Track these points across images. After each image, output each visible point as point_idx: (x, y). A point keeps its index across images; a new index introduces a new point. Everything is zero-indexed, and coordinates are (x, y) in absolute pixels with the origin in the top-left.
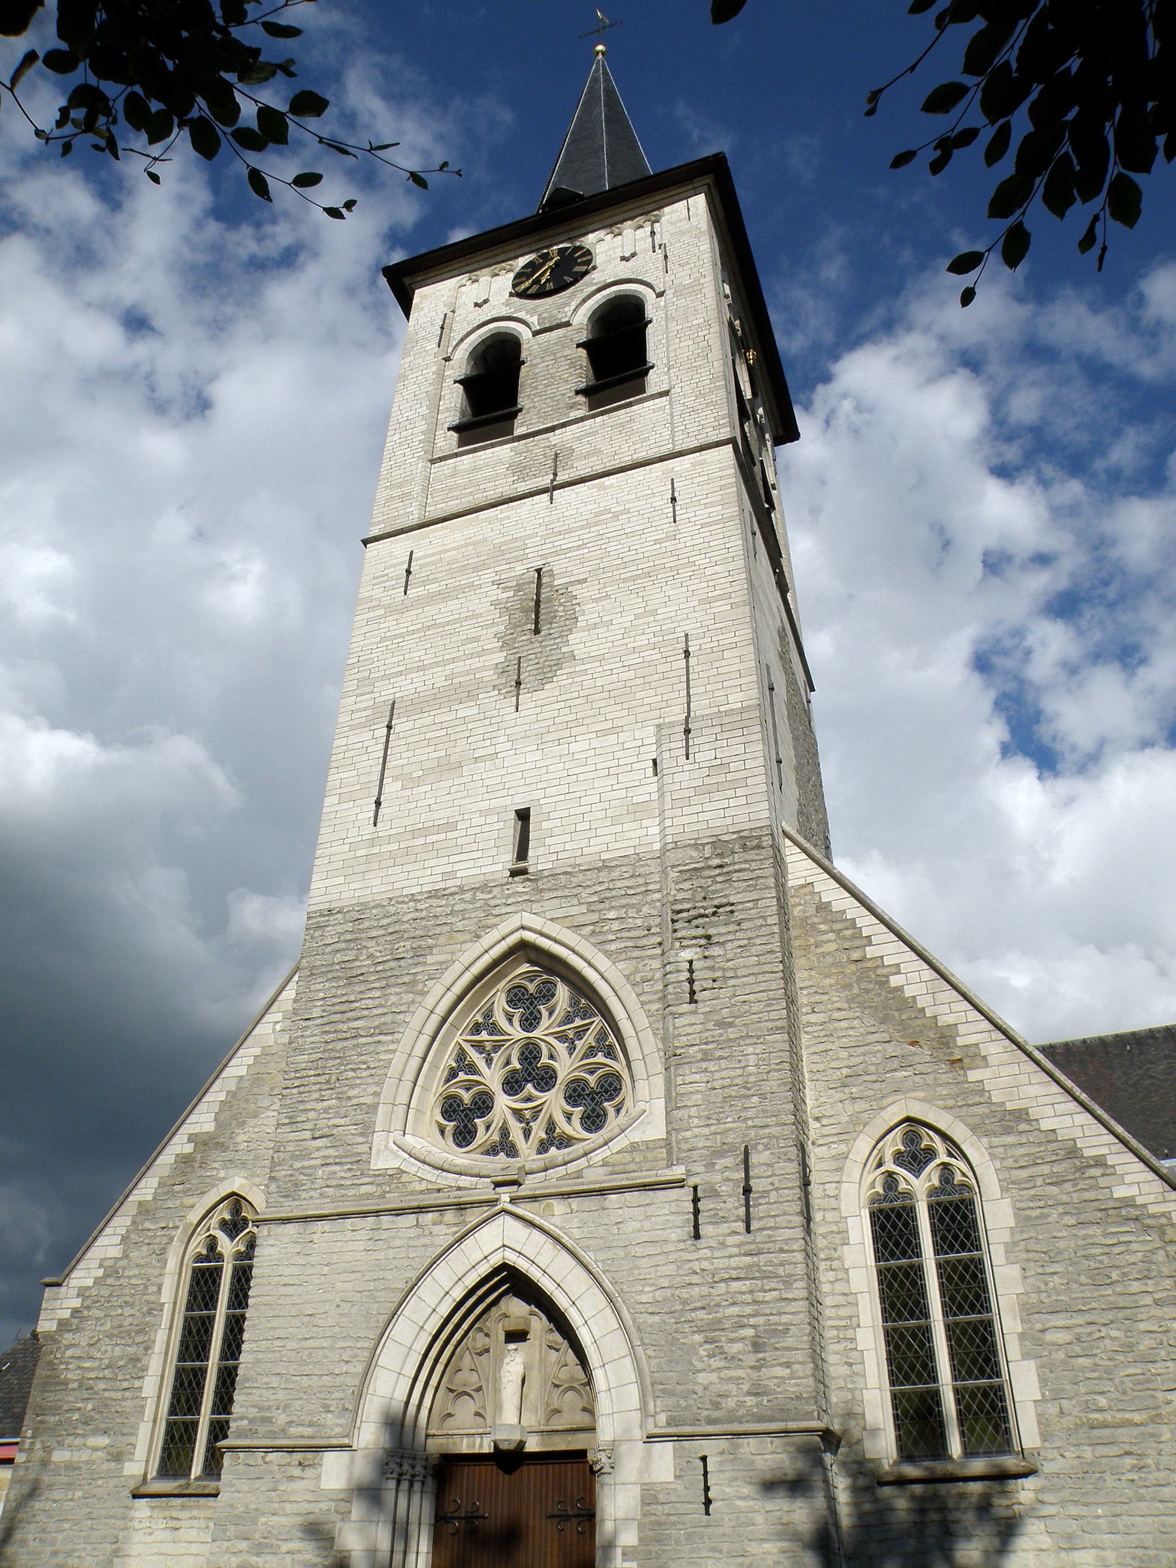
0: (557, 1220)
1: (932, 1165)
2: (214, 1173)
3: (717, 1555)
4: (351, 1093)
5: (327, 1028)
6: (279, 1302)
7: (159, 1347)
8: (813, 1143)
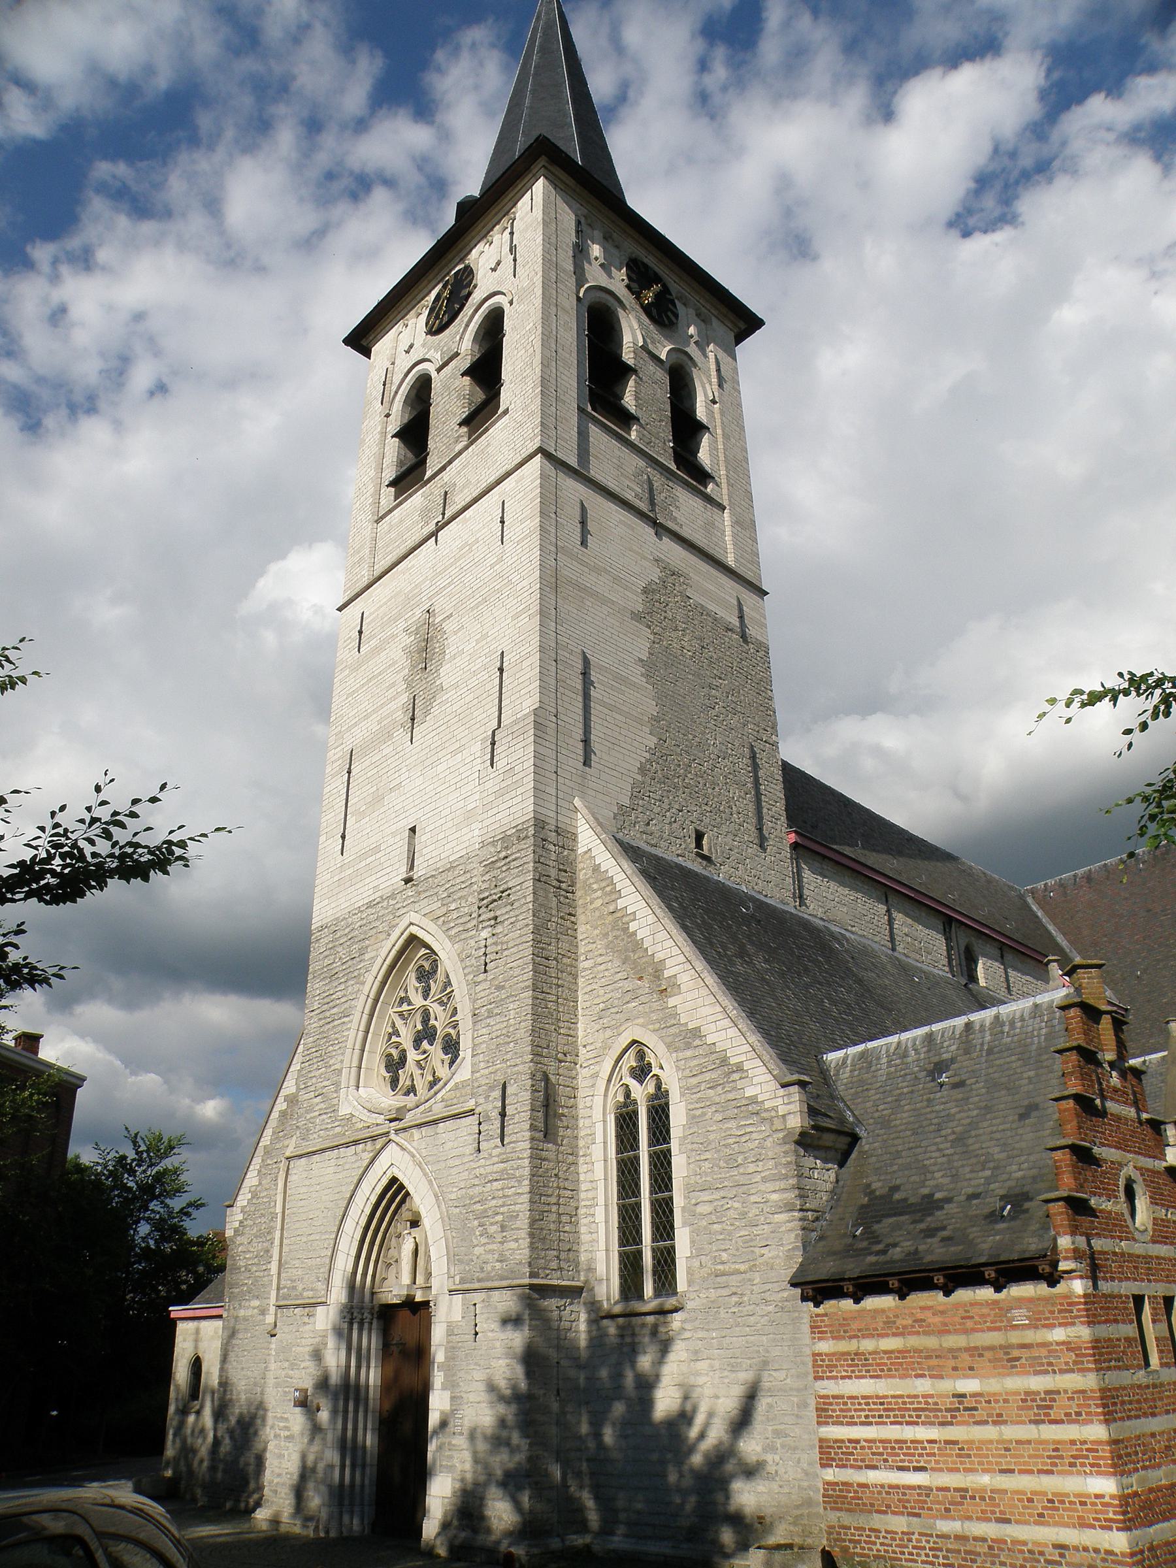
0: (415, 1144)
8: (581, 1066)
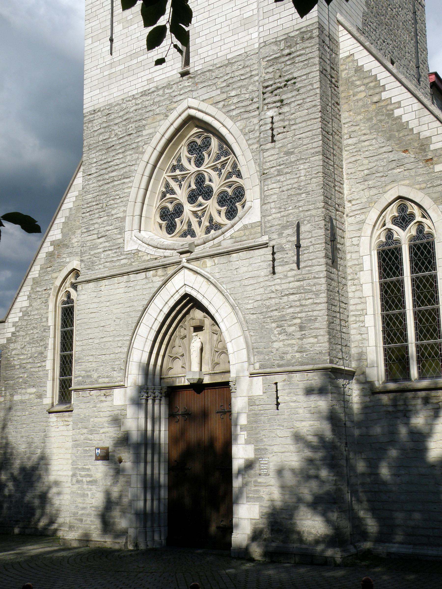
0: (208, 269)
1: (413, 223)
2: (64, 260)
3: (281, 428)
4: (113, 212)
5: (99, 178)
6: (90, 321)
7: (50, 346)
8: (347, 216)
